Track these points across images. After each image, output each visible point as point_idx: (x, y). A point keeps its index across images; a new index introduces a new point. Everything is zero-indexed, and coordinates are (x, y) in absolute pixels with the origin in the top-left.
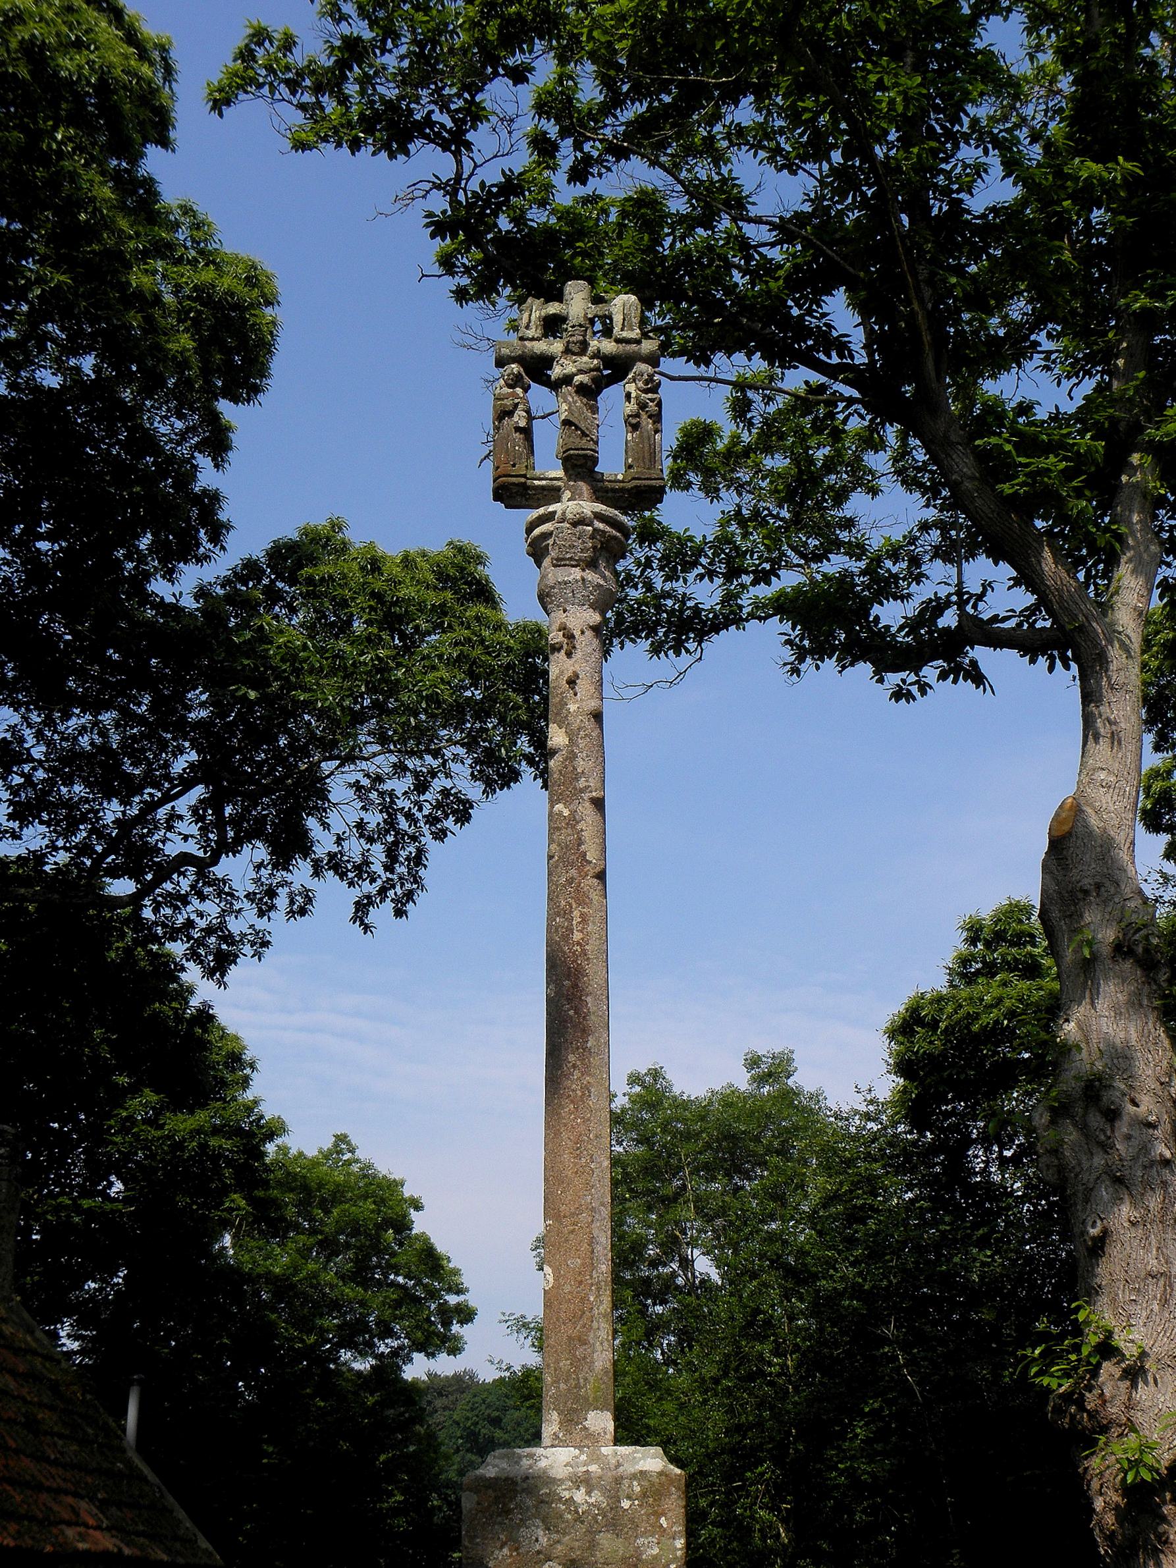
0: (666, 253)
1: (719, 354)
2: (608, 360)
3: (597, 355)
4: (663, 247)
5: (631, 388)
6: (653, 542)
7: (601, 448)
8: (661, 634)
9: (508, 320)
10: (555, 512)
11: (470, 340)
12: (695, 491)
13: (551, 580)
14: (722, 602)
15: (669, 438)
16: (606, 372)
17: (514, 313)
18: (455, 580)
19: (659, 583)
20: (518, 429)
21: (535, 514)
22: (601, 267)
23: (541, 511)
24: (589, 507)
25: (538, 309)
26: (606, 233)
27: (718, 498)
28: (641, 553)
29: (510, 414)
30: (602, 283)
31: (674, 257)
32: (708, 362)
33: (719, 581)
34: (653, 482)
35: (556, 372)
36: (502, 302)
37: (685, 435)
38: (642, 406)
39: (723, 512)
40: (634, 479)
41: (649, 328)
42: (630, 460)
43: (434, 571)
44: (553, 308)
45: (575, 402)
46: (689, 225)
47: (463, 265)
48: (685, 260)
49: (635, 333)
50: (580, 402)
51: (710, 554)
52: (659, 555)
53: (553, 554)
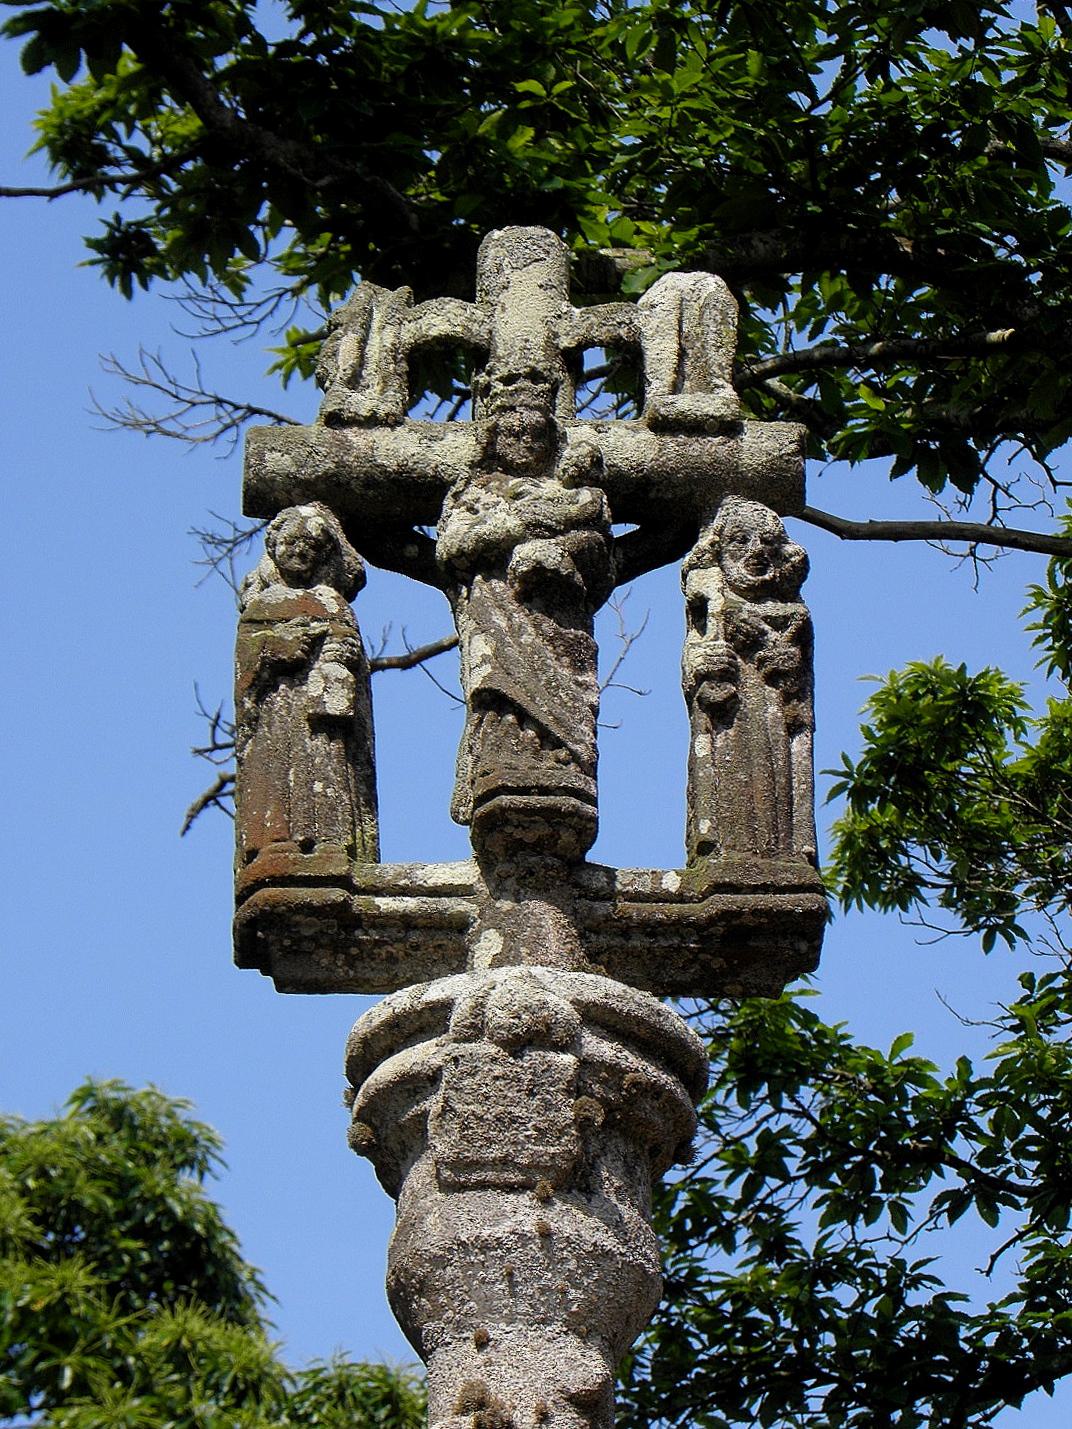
0: (825, 109)
1: (1008, 447)
2: (629, 492)
3: (591, 472)
4: (811, 91)
5: (708, 582)
6: (787, 1084)
7: (605, 787)
8: (815, 1404)
9: (280, 351)
10: (445, 1007)
11: (159, 407)
12: (932, 910)
13: (433, 1234)
14: (1031, 1291)
15: (844, 727)
16: (619, 530)
17: (308, 314)
18: (99, 1223)
19: (806, 1222)
20: (323, 723)
21: (379, 1009)
22: (602, 161)
23: (402, 999)
24: (561, 986)
25: (387, 322)
26: (618, 48)
27: (1012, 931)
28: (742, 1121)
29: (295, 671)
30: (605, 214)
31: (849, 127)
32: (967, 474)
33: (1015, 1218)
34: (785, 901)
35: (453, 531)
36: (264, 278)
37: (893, 720)
38: (746, 643)
39: (1028, 980)
40: (719, 888)
41: (769, 360)
42: (705, 826)
43: (24, 1192)
44: (442, 318)
45: (517, 631)
46: (897, 21)
47: (135, 155)
48: (890, 140)
49: (721, 400)
50: (530, 630)
51: (984, 1122)
52: (807, 1130)
53: (442, 1145)
